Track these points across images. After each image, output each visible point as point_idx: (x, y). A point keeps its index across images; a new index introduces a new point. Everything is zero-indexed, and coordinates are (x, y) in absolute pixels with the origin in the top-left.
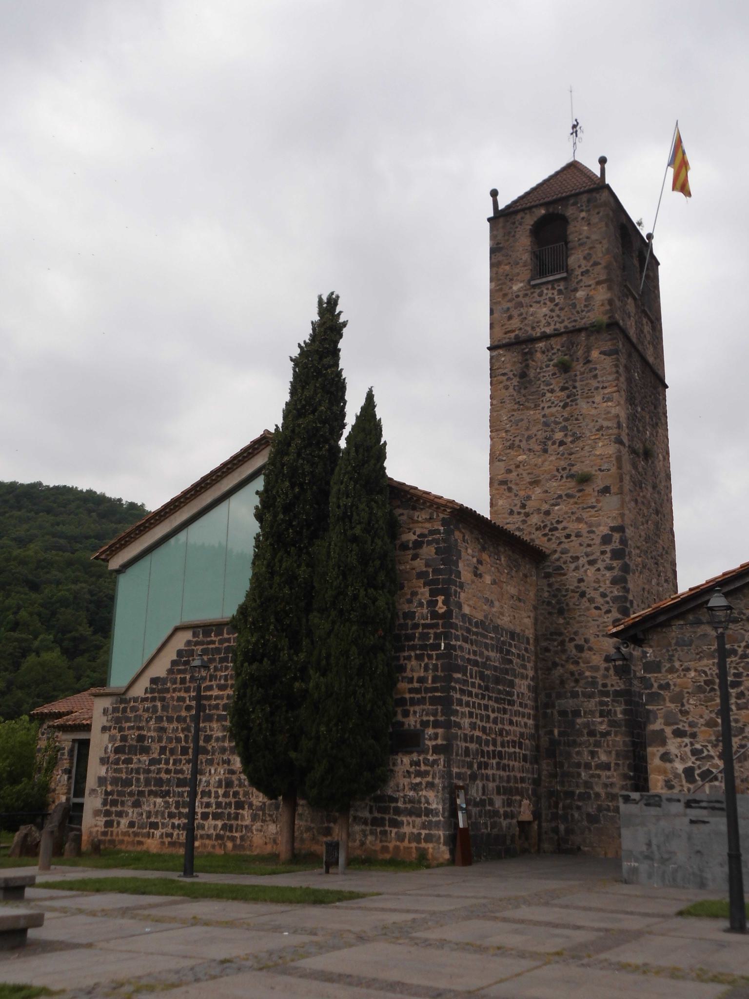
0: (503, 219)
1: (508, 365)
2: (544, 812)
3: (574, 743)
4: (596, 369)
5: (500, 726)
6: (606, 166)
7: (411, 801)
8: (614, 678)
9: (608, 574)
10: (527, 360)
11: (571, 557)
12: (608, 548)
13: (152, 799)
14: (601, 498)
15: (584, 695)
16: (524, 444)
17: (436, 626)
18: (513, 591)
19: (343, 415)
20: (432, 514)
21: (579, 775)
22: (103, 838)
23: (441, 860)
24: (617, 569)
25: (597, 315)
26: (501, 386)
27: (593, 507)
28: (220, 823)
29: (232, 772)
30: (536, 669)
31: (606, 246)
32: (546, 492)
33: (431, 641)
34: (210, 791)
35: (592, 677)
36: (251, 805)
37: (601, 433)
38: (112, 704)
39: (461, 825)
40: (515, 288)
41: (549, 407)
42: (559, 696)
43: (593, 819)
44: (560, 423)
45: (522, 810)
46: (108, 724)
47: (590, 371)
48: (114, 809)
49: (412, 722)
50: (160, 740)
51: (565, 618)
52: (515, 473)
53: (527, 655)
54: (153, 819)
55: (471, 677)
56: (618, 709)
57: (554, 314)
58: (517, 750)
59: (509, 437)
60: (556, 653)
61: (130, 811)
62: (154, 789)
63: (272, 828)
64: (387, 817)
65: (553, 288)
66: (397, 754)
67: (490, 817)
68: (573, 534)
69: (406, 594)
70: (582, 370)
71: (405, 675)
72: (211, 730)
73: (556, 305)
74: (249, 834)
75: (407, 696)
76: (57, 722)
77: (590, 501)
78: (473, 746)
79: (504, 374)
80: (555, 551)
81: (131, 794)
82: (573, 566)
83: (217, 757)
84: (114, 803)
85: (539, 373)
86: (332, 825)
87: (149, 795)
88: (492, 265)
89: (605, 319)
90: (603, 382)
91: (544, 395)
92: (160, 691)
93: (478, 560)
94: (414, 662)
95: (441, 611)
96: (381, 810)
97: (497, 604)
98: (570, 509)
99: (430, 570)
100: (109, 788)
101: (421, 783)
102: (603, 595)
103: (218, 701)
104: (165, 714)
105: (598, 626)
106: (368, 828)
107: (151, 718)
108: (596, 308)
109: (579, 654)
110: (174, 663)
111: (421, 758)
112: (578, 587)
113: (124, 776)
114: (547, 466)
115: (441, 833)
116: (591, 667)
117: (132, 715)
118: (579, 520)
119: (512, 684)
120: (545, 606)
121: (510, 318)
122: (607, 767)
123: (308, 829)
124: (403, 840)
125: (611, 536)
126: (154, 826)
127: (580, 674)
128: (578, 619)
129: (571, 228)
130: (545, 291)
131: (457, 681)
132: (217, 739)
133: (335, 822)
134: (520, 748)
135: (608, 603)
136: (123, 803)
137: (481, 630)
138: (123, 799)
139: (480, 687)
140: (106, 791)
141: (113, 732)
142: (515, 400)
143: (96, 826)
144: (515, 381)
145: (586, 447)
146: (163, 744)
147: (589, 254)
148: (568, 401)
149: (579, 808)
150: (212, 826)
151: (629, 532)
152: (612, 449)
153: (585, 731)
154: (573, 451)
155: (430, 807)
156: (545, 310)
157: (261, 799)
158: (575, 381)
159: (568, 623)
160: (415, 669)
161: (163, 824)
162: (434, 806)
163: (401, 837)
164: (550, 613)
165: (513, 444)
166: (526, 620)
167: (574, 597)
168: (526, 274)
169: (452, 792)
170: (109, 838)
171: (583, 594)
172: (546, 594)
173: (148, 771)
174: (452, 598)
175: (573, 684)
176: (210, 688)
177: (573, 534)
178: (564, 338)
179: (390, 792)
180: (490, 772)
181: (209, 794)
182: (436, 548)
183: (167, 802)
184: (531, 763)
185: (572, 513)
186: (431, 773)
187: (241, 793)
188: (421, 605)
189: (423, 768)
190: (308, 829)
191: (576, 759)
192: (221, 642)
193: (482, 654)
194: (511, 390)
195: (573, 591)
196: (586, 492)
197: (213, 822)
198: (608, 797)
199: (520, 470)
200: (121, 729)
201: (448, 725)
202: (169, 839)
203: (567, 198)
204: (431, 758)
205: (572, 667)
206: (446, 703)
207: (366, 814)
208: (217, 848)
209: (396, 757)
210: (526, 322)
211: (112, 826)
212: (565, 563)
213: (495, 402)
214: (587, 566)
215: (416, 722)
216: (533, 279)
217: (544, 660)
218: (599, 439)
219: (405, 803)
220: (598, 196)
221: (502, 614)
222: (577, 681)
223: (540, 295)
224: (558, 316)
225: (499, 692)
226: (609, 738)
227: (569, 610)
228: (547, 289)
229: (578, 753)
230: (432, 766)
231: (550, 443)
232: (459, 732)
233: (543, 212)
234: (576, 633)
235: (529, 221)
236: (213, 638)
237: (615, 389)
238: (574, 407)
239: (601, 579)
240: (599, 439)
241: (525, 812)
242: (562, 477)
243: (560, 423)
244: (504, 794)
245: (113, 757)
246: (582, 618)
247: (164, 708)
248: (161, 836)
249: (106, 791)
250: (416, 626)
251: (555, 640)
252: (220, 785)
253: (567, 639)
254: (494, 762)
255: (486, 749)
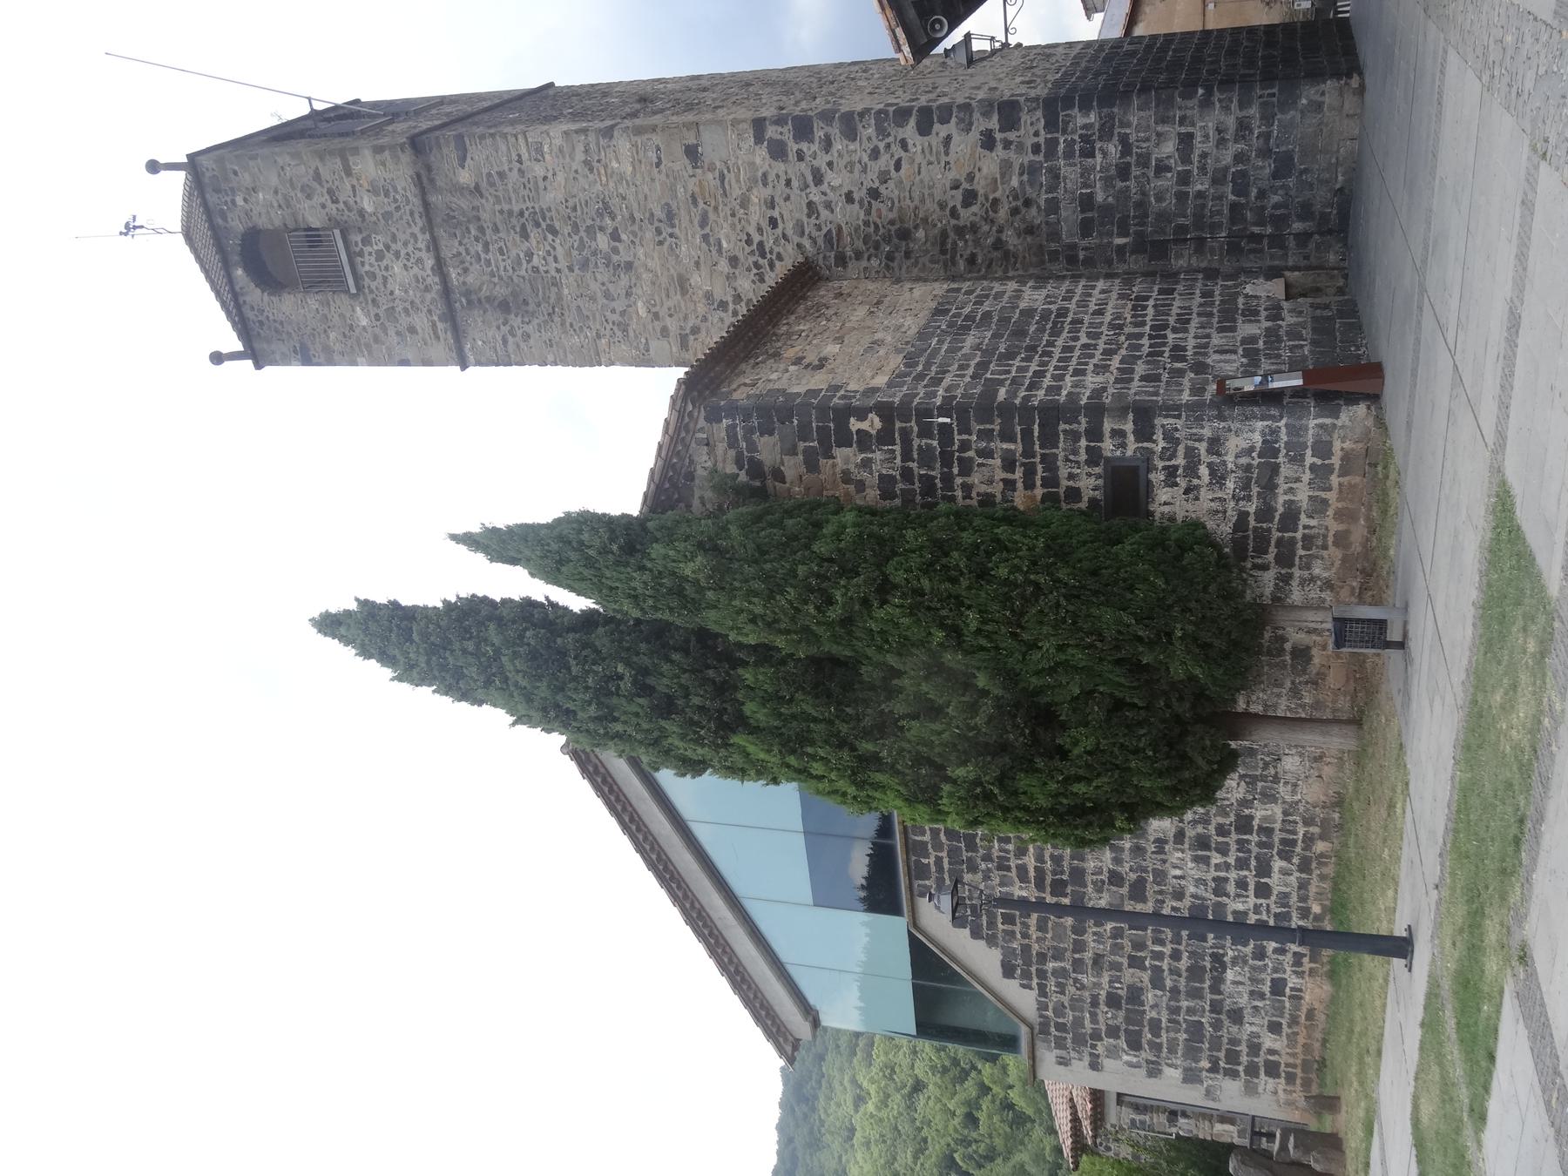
0: (259, 343)
1: (490, 334)
2: (1268, 263)
3: (1141, 205)
4: (489, 175)
5: (1104, 328)
6: (162, 161)
7: (1246, 486)
8: (1022, 132)
9: (838, 146)
10: (479, 301)
11: (809, 216)
12: (793, 147)
13: (1227, 987)
14: (707, 161)
15: (1052, 188)
16: (619, 305)
17: (905, 434)
18: (861, 312)
19: (528, 603)
20: (699, 442)
21: (1200, 195)
22: (1298, 1081)
23: (1370, 422)
24: (828, 129)
25: (401, 173)
26: (522, 345)
27: (722, 177)
28: (1278, 864)
29: (1180, 836)
30: (1005, 279)
31: (288, 159)
32: (697, 264)
33: (935, 443)
34: (1214, 879)
35: (1021, 174)
36: (1244, 803)
37: (595, 164)
38: (1049, 1049)
39: (1300, 382)
40: (364, 322)
41: (556, 260)
42: (1054, 235)
43: (1284, 166)
44: (581, 239)
45: (1263, 294)
46: (1087, 1059)
47: (492, 184)
48: (1244, 1059)
49: (1089, 484)
50: (1116, 967)
51: (916, 227)
52: (669, 322)
53: (978, 292)
54: (1266, 989)
55: (1008, 372)
56: (1081, 120)
57: (403, 253)
58: (1151, 303)
59: (608, 332)
60: (977, 242)
61: (1248, 1029)
62: (1208, 983)
63: (1291, 764)
64: (1276, 535)
65: (361, 254)
66: (1152, 514)
67: (1279, 340)
68: (770, 213)
69: (847, 494)
70: (491, 200)
71: (999, 498)
72: (1099, 871)
73: (388, 248)
74: (1302, 809)
75: (1039, 492)
76: (1087, 1129)
77: (713, 183)
78: (1140, 368)
79: (505, 341)
80: (799, 246)
81: (1217, 1025)
82: (824, 213)
83: (1151, 862)
84: (1233, 1057)
85: (501, 278)
86: (1288, 646)
87: (1220, 993)
88: (330, 362)
89: (406, 157)
90: (510, 162)
91: (536, 270)
92: (1028, 963)
93: (794, 364)
94: (975, 479)
95: (878, 424)
96: (1262, 550)
97: (878, 336)
98: (726, 220)
99: (802, 445)
100: (1205, 1064)
101: (1210, 465)
102: (875, 154)
103: (1047, 858)
104: (1068, 954)
105: (930, 163)
106: (1297, 572)
107: (1076, 980)
108: (388, 176)
109: (981, 199)
110: (976, 934)
111: (1160, 464)
112: (861, 202)
113: (1183, 1036)
114: (655, 264)
115: (1312, 423)
116: (1003, 175)
117: (1070, 1015)
118: (745, 203)
119: (1028, 313)
120: (895, 264)
121: (412, 330)
122: (1186, 140)
123: (1295, 692)
124: (1325, 502)
125: (771, 141)
126: (1278, 987)
127: (1016, 198)
128: (916, 202)
129: (262, 223)
130: (367, 268)
131: (1012, 394)
132: (1117, 861)
133: (1283, 639)
134: (1147, 298)
135: (888, 146)
136: (1234, 1041)
137: (922, 359)
138: (1225, 1040)
139: (1028, 359)
140: (1210, 1070)
141: (1100, 1049)
142: (545, 322)
143: (1276, 1093)
144: (516, 321)
145: (621, 191)
146: (1125, 961)
147: (302, 190)
148: (544, 225)
149: (1262, 194)
150: (1282, 877)
151: (768, 112)
152: (623, 144)
153: (1120, 184)
154: (627, 215)
155: (1259, 445)
156: (397, 268)
157: (1234, 784)
158: (510, 213)
159: (925, 220)
160: (987, 478)
161: (1275, 970)
162: (1257, 438)
163: (1319, 506)
164: (908, 255)
165: (619, 325)
166: (917, 293)
167: (879, 210)
168: (342, 301)
169: (1230, 400)
170: (1298, 1071)
171: (874, 194)
172: (875, 262)
173: (1175, 991)
174: (855, 402)
175: (1034, 211)
176: (1022, 871)
177: (770, 213)
178: (441, 233)
179: (1227, 528)
180: (1191, 343)
181: (1220, 882)
182: (762, 435)
183: (1235, 961)
184: (1177, 283)
185: (733, 215)
186: (1190, 443)
187: (1220, 820)
188: (866, 464)
189: (1180, 461)
190: (1295, 692)
191: (1170, 202)
192: (938, 846)
193: (967, 357)
194: (529, 328)
195: (868, 213)
196: (697, 189)
197: (1276, 875)
198: (1244, 137)
199: (663, 312)
200: (1096, 1036)
201: (1096, 411)
202: (1306, 960)
203: (213, 227)
204: (1162, 444)
205: (1003, 214)
206: (1053, 415)
207: (1269, 578)
208: (1325, 870)
209: (1157, 516)
210: (417, 301)
211: (1277, 1064)
212: (819, 228)
213: (550, 358)
214: (825, 187)
215: (1089, 475)
216: (347, 291)
217: (989, 266)
218: (606, 167)
219: (1249, 498)
220: (208, 174)
221: (898, 328)
222: (1028, 203)
223: (373, 276)
224: (405, 244)
225: (1041, 330)
226: (1132, 138)
227: (902, 221)
228: (363, 264)
229: (1159, 199)
230: (1177, 442)
231: (615, 258)
232: (1111, 390)
233: (240, 272)
234: (942, 206)
235: (255, 295)
236: (932, 860)
237: (521, 140)
238: (553, 213)
239: (846, 159)
240: (606, 167)
241: (1266, 290)
242: (671, 235)
243: (581, 239)
244: (1235, 321)
245: (1146, 1054)
246: (916, 195)
247: (1058, 956)
248: (1300, 974)
249: (1210, 1070)
250: (907, 474)
251: (954, 243)
252: (1206, 861)
253: (953, 222)
254: (1171, 336)
255: (1146, 350)
